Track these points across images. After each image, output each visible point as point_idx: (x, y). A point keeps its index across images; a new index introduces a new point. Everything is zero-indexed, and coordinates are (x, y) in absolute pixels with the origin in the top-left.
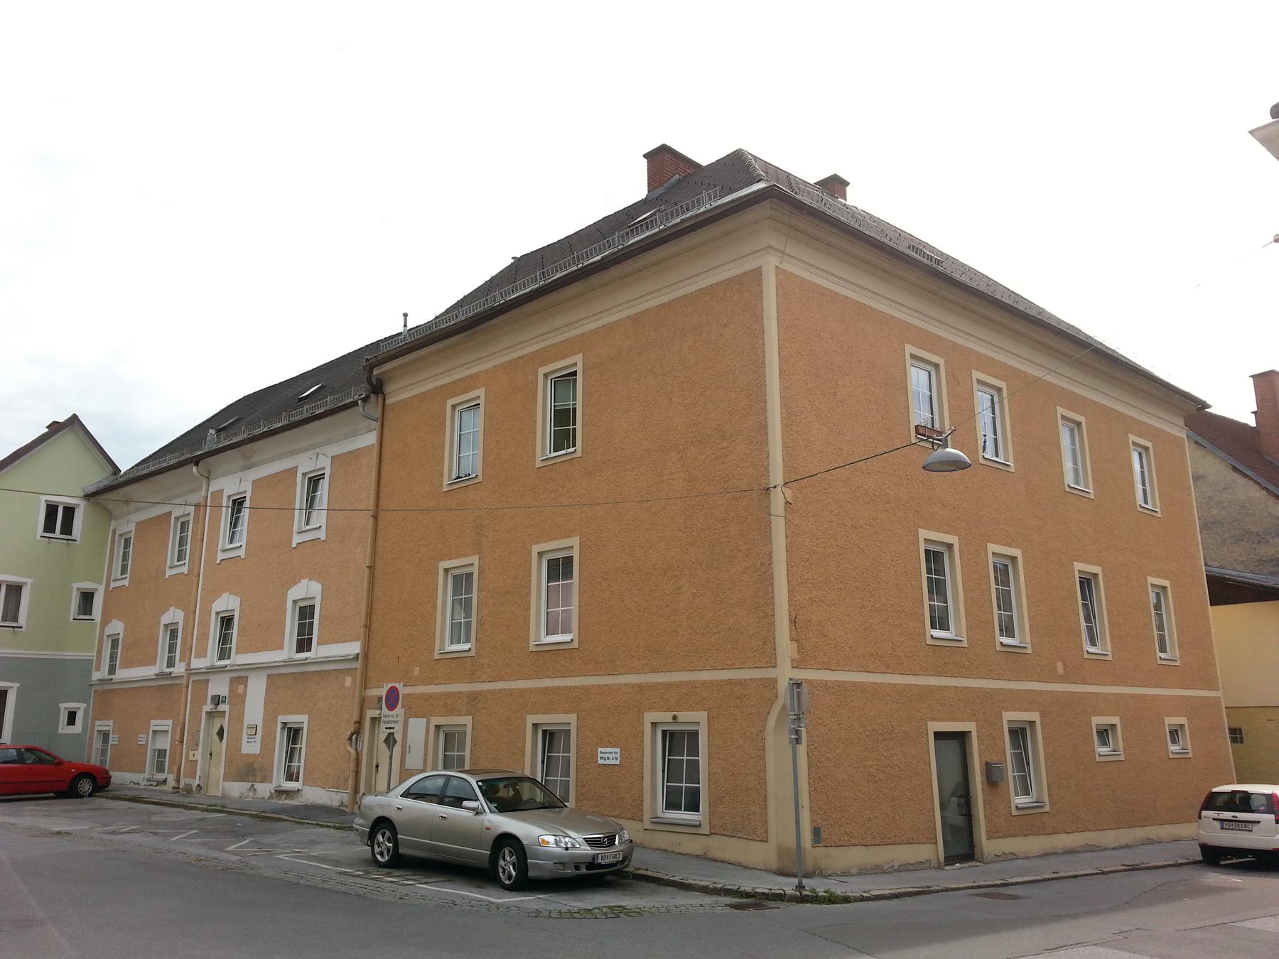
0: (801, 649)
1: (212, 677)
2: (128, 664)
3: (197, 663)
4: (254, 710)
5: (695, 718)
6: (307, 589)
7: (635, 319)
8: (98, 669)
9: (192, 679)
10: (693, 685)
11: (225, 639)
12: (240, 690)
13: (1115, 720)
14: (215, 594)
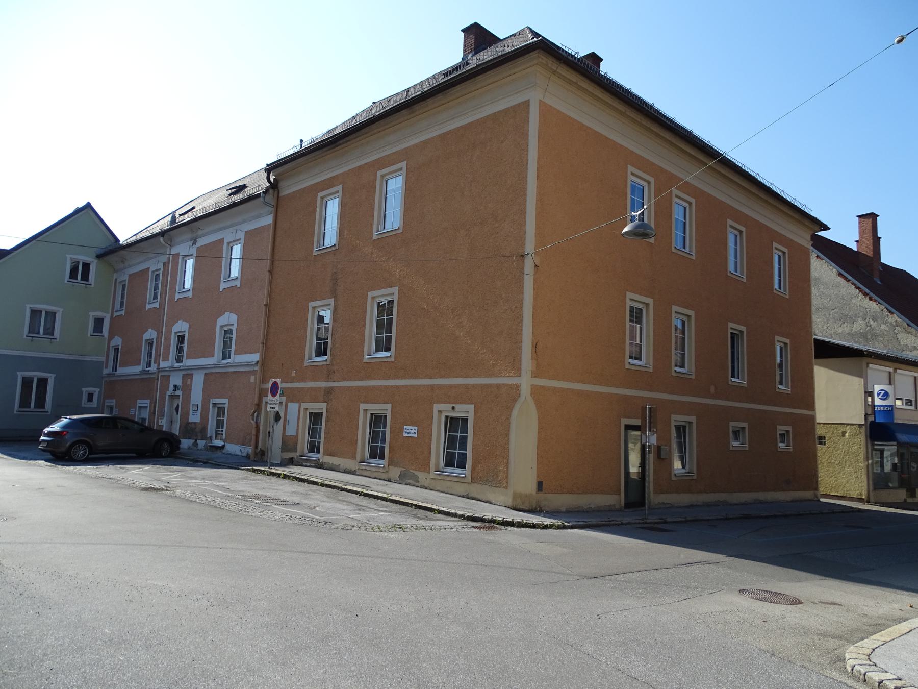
0: (538, 365)
1: (172, 374)
2: (124, 364)
3: (163, 365)
4: (197, 396)
5: (466, 410)
6: (229, 319)
7: (443, 137)
8: (106, 367)
9: (161, 374)
10: (466, 386)
11: (180, 350)
12: (189, 383)
13: (745, 425)
14: (173, 320)
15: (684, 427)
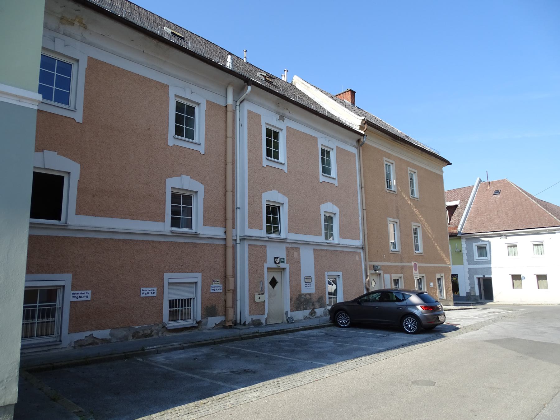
1: (268, 245)
15: (398, 280)
